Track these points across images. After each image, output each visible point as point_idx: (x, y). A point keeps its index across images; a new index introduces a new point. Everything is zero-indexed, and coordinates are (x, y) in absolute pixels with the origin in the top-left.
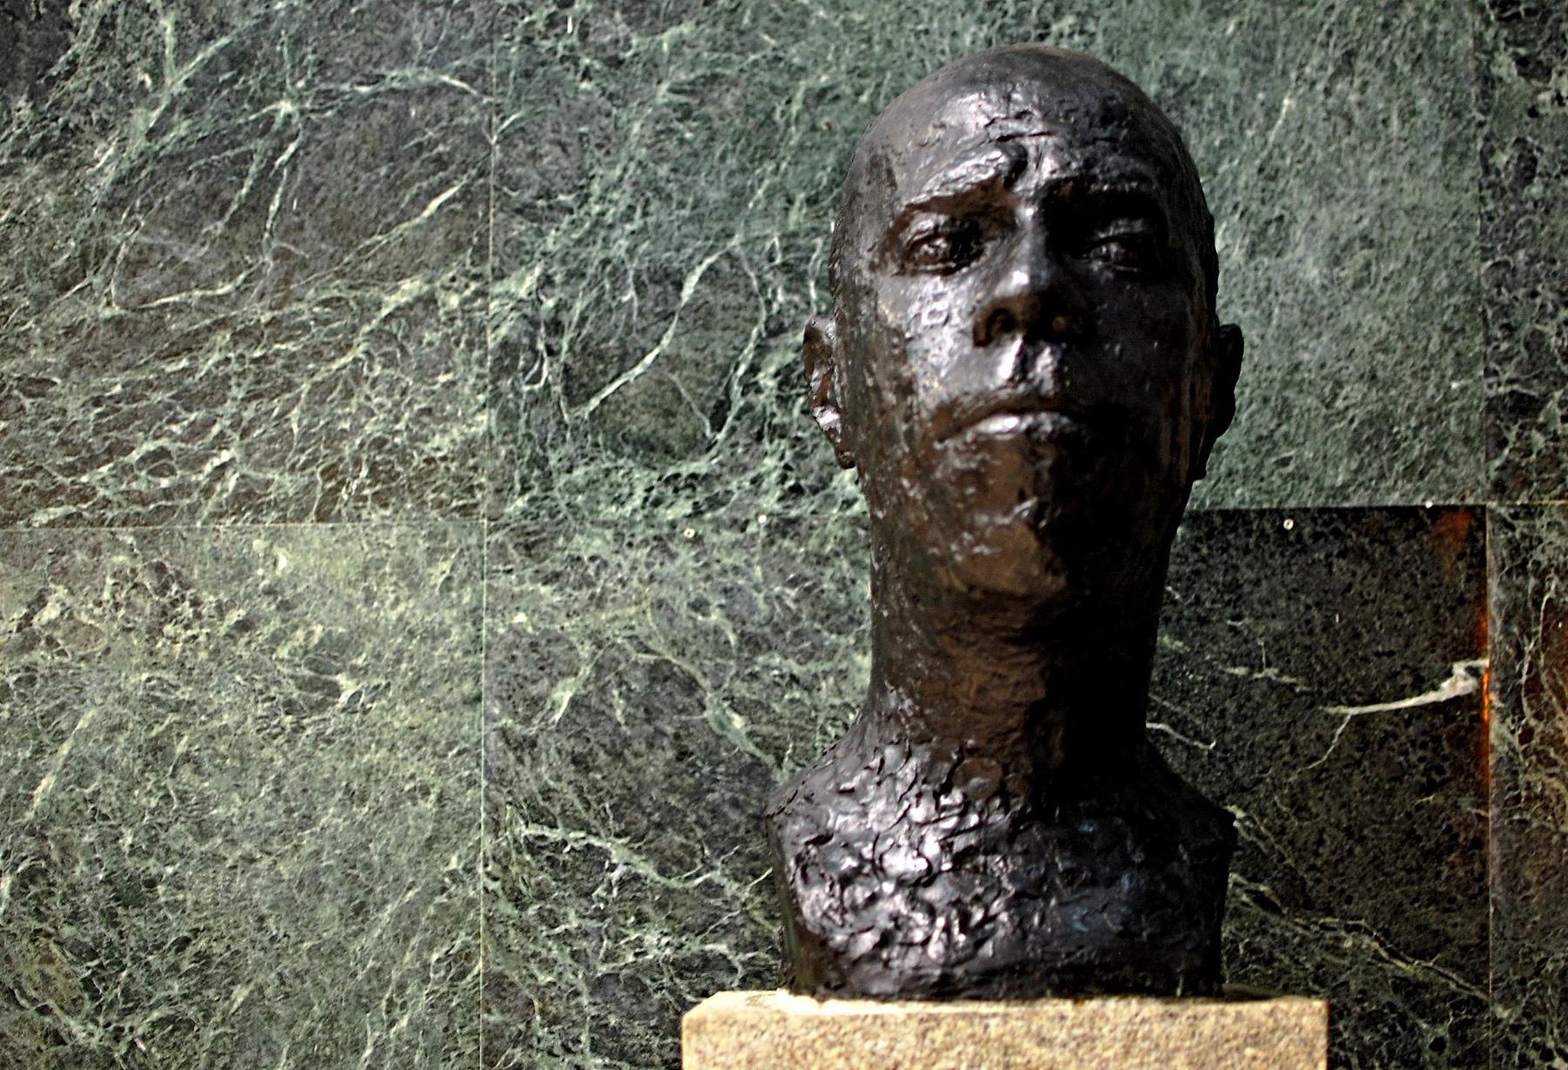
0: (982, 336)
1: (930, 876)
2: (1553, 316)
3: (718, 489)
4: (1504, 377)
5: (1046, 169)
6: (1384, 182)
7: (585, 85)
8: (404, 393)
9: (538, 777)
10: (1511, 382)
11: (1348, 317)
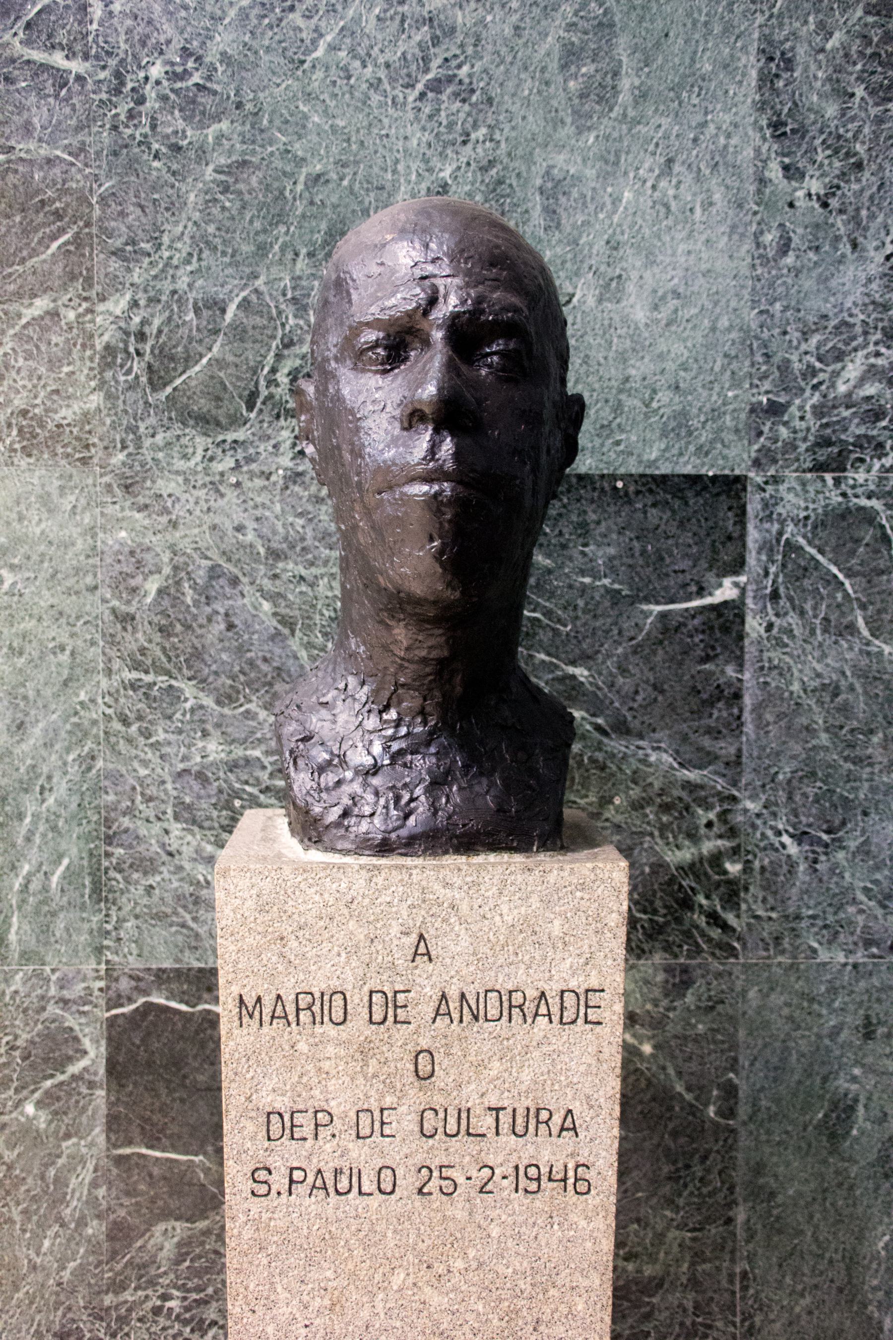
0: (406, 425)
1: (375, 769)
2: (797, 348)
3: (251, 451)
4: (763, 389)
5: (450, 304)
6: (689, 252)
7: (156, 164)
8: (40, 378)
9: (136, 640)
10: (767, 392)
11: (662, 347)
